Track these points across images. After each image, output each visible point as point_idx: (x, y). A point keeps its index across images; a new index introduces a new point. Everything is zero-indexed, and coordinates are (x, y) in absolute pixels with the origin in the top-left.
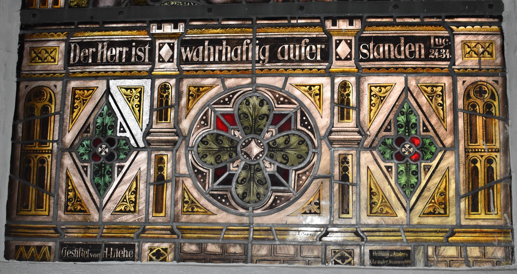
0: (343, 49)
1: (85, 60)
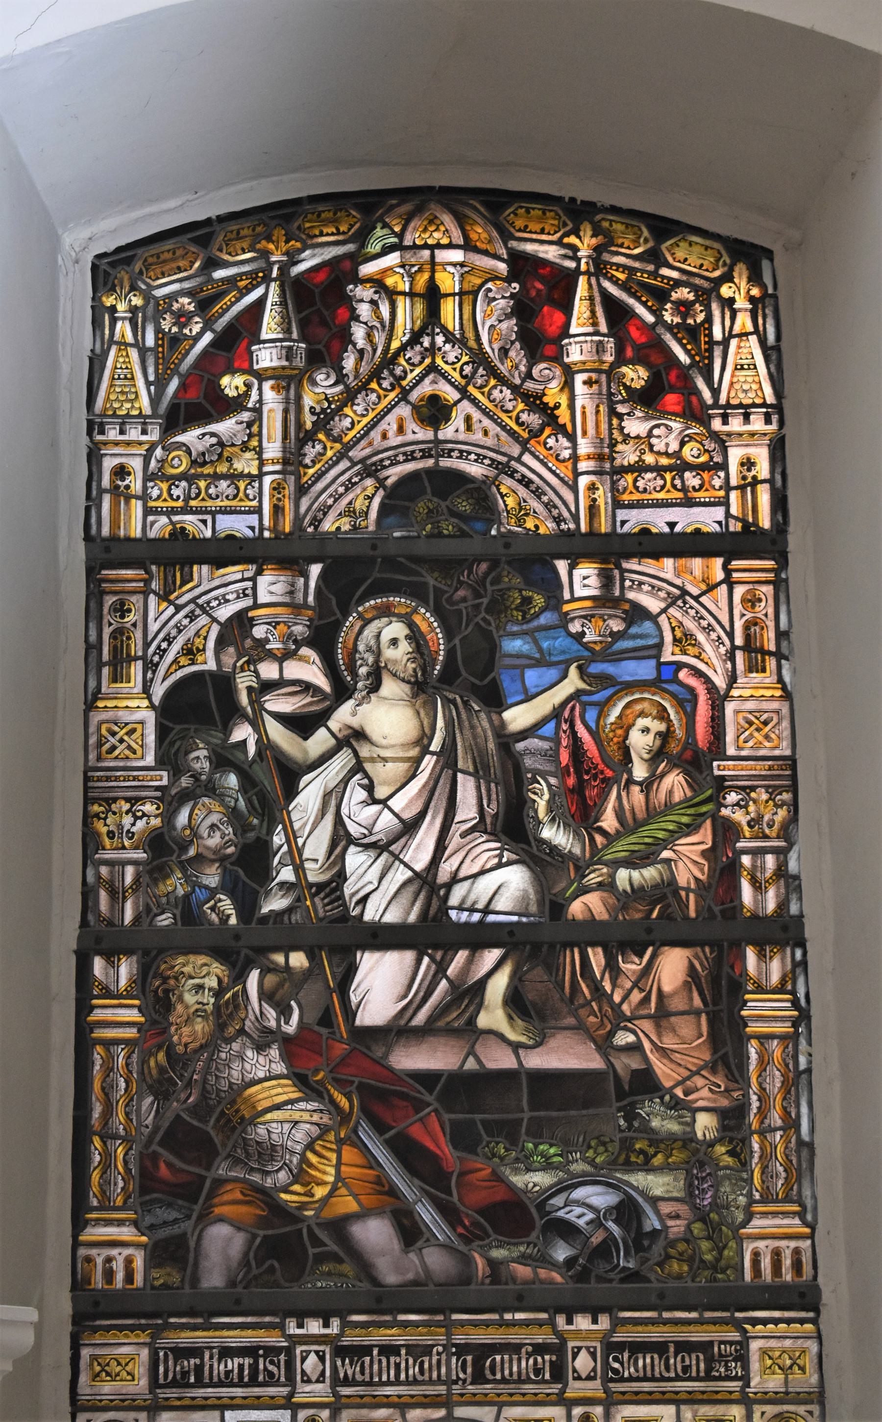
0: (583, 1362)
1: (183, 1378)
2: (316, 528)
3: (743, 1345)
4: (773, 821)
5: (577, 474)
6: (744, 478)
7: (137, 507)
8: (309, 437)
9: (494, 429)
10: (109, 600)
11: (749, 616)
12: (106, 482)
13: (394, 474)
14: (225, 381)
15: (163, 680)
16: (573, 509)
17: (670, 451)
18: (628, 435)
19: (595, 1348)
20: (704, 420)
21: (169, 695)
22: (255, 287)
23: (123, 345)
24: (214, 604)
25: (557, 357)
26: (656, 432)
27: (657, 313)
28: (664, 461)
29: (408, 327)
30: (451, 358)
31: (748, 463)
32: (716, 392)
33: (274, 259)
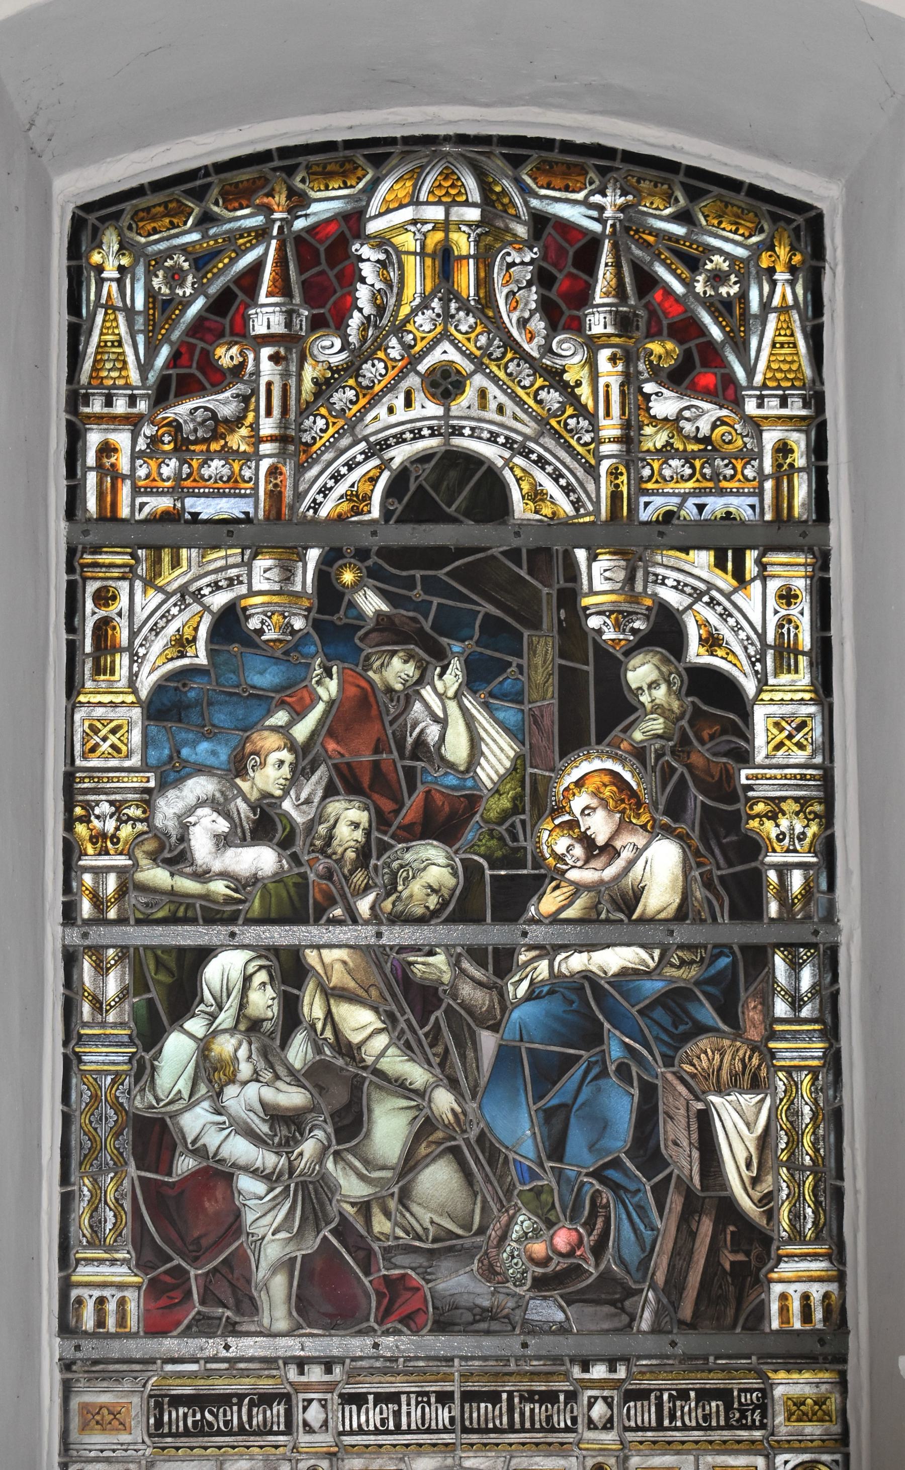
2: (316, 511)
3: (765, 1393)
4: (804, 833)
5: (600, 459)
6: (780, 466)
7: (125, 490)
8: (307, 410)
9: (510, 406)
10: (92, 587)
11: (783, 612)
12: (91, 460)
13: (400, 455)
14: (220, 351)
15: (150, 673)
16: (593, 496)
17: (700, 435)
18: (655, 417)
19: (612, 1397)
20: (737, 403)
21: (158, 689)
22: (253, 247)
23: (109, 307)
24: (206, 591)
25: (577, 326)
26: (687, 414)
27: (689, 285)
28: (693, 447)
29: (418, 291)
30: (464, 328)
31: (783, 449)
32: (751, 372)
33: (277, 215)
